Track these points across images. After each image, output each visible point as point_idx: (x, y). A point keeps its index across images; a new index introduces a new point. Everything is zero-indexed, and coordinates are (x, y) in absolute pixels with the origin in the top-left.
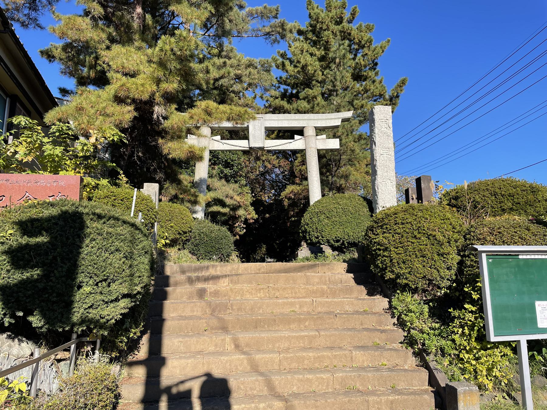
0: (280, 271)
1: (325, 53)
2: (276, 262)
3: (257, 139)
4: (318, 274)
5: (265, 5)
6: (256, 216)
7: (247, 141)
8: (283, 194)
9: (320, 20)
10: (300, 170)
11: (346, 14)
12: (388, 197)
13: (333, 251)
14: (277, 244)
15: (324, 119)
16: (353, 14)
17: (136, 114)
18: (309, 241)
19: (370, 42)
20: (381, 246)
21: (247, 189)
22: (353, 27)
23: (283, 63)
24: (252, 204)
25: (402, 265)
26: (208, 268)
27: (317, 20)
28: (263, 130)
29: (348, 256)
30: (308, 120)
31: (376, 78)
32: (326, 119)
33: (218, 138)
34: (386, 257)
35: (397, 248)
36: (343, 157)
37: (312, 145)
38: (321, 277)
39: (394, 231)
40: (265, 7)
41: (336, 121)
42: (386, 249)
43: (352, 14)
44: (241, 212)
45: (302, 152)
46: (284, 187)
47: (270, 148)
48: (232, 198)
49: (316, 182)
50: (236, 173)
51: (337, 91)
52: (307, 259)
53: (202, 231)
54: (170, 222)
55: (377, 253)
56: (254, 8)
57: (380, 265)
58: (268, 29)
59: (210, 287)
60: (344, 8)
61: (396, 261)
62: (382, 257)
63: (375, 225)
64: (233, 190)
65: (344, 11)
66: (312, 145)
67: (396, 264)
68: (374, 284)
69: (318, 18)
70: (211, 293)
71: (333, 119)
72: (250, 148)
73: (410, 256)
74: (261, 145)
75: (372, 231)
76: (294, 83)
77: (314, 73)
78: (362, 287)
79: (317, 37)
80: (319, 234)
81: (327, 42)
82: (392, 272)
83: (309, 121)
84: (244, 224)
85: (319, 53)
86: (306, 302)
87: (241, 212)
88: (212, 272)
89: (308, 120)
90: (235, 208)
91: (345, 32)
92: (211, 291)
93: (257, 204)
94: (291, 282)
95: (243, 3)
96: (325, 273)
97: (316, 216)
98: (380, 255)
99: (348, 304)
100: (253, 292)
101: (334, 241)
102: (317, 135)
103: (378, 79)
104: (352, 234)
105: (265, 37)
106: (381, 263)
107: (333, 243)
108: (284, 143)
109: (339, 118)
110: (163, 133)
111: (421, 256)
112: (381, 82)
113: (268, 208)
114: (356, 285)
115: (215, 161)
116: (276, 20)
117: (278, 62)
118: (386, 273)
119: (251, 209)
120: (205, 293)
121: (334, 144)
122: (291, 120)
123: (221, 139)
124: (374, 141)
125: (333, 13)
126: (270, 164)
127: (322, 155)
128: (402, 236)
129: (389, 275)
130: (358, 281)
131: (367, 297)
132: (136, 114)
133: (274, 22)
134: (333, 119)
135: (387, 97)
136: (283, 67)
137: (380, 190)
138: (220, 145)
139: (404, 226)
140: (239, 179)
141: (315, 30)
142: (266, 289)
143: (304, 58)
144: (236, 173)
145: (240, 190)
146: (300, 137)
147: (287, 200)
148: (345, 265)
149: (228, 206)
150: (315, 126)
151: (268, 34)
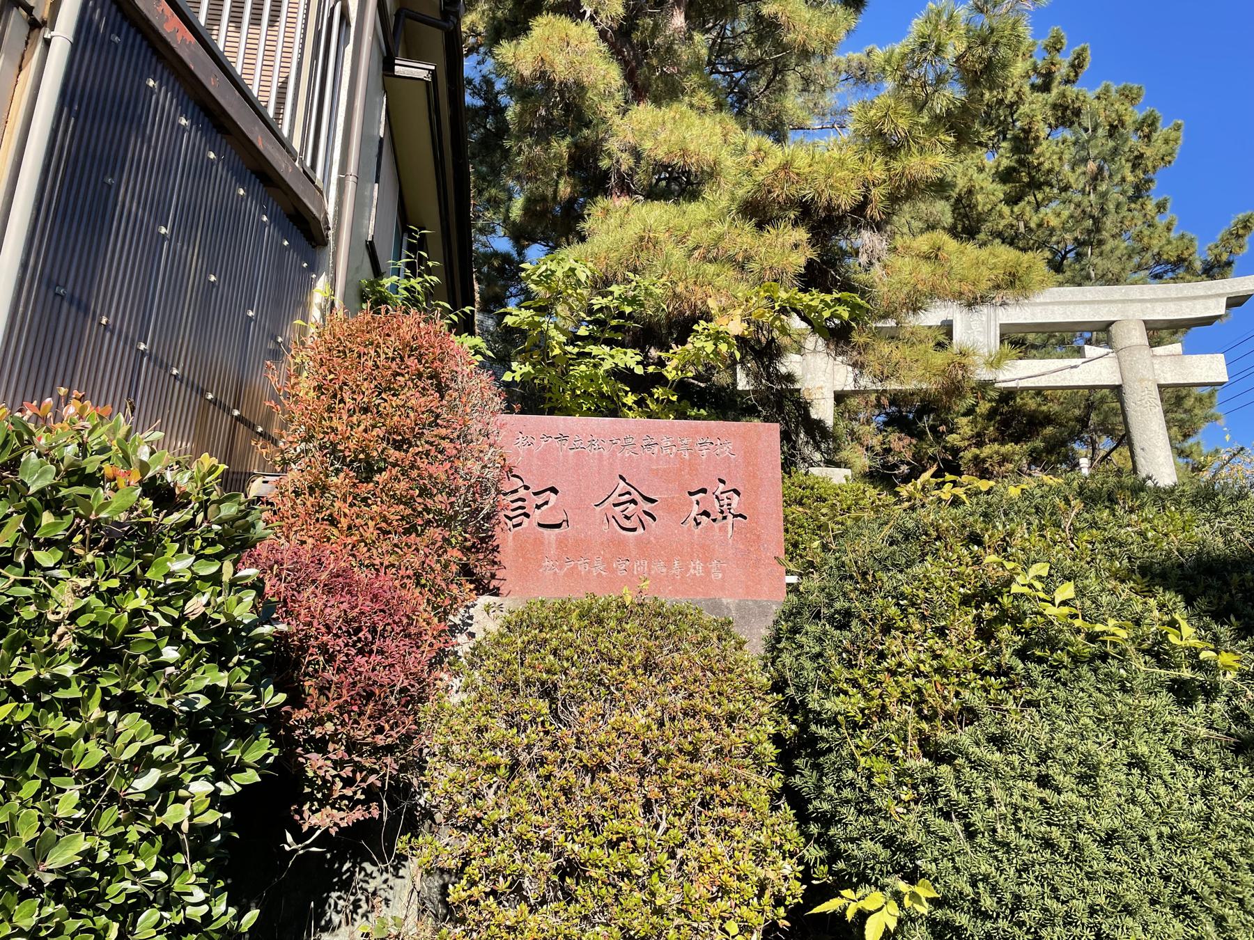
15: (1173, 300)
30: (1123, 301)
47: (1012, 384)
60: (1058, 50)
65: (1058, 58)
71: (1202, 299)
81: (1027, 131)
83: (1136, 303)
89: (1123, 301)
91: (1067, 108)
109: (1219, 295)
121: (1209, 368)
122: (1070, 303)
127: (1175, 398)
135: (1198, 265)
150: (1146, 318)
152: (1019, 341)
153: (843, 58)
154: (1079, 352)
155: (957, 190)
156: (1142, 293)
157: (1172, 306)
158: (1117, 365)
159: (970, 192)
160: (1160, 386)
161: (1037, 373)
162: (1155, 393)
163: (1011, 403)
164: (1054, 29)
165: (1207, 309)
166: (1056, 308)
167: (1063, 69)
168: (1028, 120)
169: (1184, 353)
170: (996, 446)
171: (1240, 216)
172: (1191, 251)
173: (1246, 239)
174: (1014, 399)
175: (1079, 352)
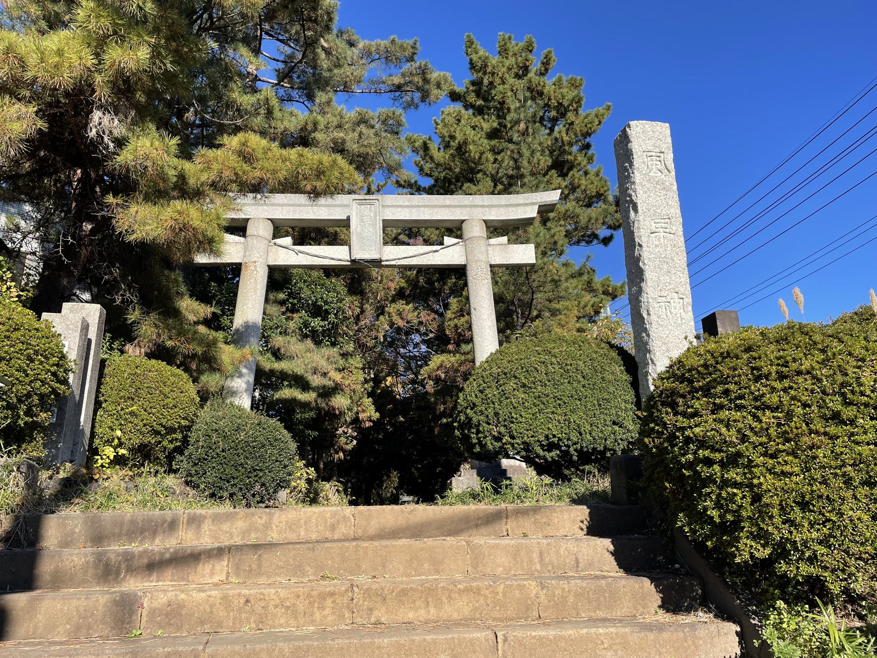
0: (394, 534)
1: (500, 124)
2: (417, 503)
3: (366, 244)
4: (505, 541)
5: (392, 37)
6: (376, 416)
7: (346, 248)
8: (424, 372)
9: (489, 70)
10: (456, 326)
11: (535, 61)
12: (671, 335)
13: (539, 474)
15: (503, 206)
16: (546, 64)
17: (42, 124)
18: (478, 449)
19: (579, 101)
20: (713, 449)
21: (357, 362)
22: (547, 82)
25: (797, 514)
26: (172, 525)
27: (484, 68)
28: (380, 225)
29: (580, 486)
30: (471, 206)
31: (589, 167)
32: (507, 206)
33: (288, 241)
34: (735, 485)
35: (773, 456)
36: (538, 296)
37: (483, 258)
38: (517, 550)
39: (756, 399)
40: (393, 41)
41: (528, 208)
42: (733, 460)
43: (543, 63)
45: (460, 272)
48: (325, 375)
49: (488, 331)
50: (335, 326)
51: (522, 176)
52: (474, 496)
53: (215, 426)
54: (129, 402)
55: (697, 474)
56: (373, 43)
57: (714, 513)
58: (397, 80)
59: (156, 592)
60: (531, 51)
61: (776, 500)
62: (721, 488)
63: (683, 388)
64: (328, 359)
65: (530, 57)
66: (483, 258)
67: (775, 512)
68: (676, 573)
69: (486, 66)
70: (153, 612)
71: (522, 206)
72: (353, 261)
73: (825, 482)
74: (374, 255)
75: (673, 405)
76: (445, 178)
77: (480, 158)
78: (646, 582)
79: (485, 100)
80: (503, 430)
81: (502, 103)
82: (761, 536)
83: (474, 208)
85: (489, 123)
86: (472, 642)
88: (186, 539)
89: (471, 206)
90: (326, 393)
92: (155, 604)
93: (382, 398)
94: (426, 565)
95: (355, 37)
96: (525, 535)
97: (494, 384)
98: (711, 480)
99: (610, 648)
100: (301, 607)
101: (542, 446)
102: (489, 238)
103: (592, 169)
104: (588, 427)
105: (392, 95)
106: (718, 505)
107: (541, 453)
108: (421, 252)
109: (533, 204)
110: (125, 185)
111: (864, 483)
112: (597, 175)
113: (403, 405)
114: (621, 573)
115: (293, 305)
116: (412, 63)
117: (417, 144)
118: (738, 540)
119: (368, 401)
120: (132, 612)
121: (524, 254)
122: (435, 206)
123: (294, 244)
124: (632, 201)
125: (511, 61)
126: (402, 319)
128: (789, 415)
129: (748, 549)
130: (629, 562)
131: (664, 617)
132: (42, 124)
133: (407, 67)
135: (611, 198)
136: (425, 151)
137: (653, 317)
138: (290, 255)
139: (786, 383)
141: (480, 89)
142: (342, 595)
143: (462, 131)
144: (335, 326)
145: (341, 362)
146: (456, 240)
148: (583, 512)
149: (314, 389)
150: (485, 218)
151: (399, 88)
153: (373, 43)
155: (457, 142)
156: (483, 201)
158: (464, 250)
159: (465, 143)
160: (491, 266)
161: (411, 255)
164: (527, 37)
165: (525, 212)
167: (535, 66)
168: (502, 95)
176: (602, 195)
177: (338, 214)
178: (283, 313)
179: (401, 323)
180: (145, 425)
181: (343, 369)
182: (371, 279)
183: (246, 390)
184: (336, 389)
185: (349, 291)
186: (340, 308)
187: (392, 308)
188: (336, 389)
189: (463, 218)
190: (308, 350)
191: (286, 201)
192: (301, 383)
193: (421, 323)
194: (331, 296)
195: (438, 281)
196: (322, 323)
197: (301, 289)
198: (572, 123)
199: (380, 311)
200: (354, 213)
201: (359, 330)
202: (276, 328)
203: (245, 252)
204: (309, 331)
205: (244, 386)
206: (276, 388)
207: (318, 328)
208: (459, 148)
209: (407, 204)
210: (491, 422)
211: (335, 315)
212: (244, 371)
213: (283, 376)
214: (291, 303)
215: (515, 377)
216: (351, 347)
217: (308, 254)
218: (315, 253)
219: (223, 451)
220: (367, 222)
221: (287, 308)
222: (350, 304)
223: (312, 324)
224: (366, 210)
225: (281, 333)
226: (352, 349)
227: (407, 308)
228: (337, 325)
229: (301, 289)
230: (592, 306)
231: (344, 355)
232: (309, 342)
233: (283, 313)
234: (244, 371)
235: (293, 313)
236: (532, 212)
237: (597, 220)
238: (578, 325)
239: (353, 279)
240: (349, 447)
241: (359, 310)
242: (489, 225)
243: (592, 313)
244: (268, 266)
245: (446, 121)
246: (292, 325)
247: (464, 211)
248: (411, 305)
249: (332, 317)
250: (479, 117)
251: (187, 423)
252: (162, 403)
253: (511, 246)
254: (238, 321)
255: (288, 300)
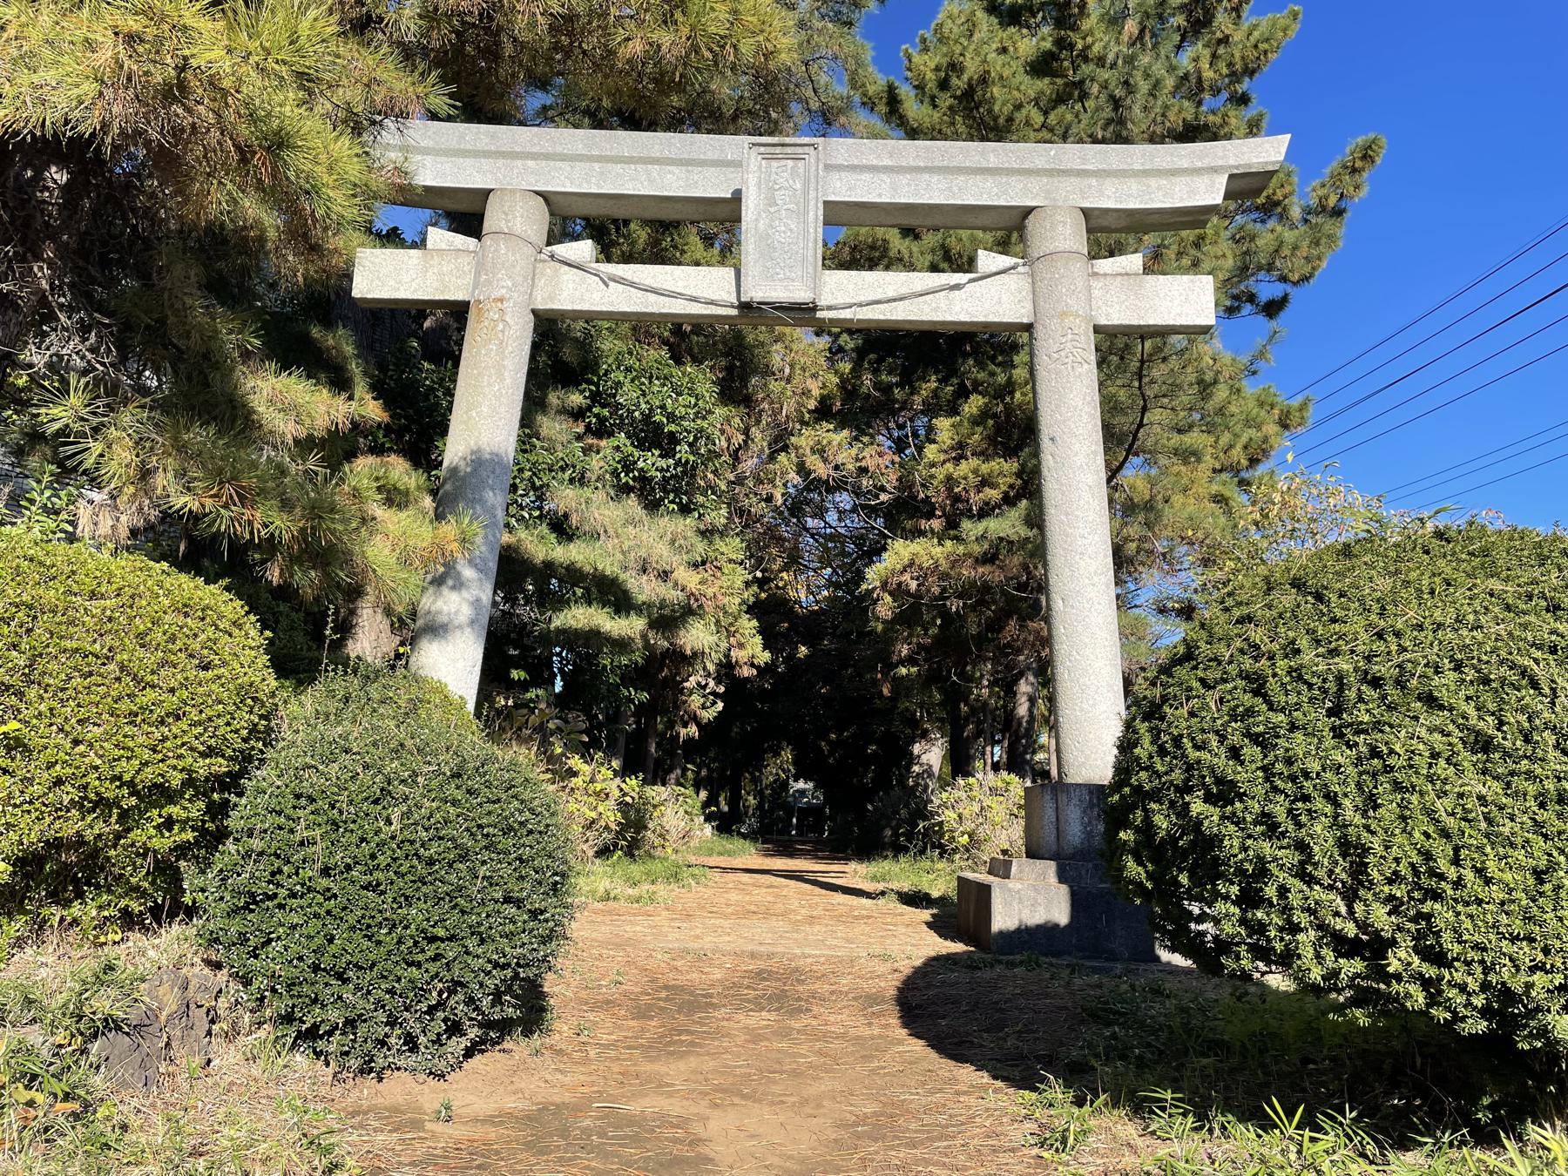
3: (780, 261)
6: (764, 657)
7: (728, 273)
8: (873, 575)
10: (949, 478)
14: (830, 742)
21: (732, 547)
23: (891, 89)
24: (754, 609)
28: (816, 214)
30: (1051, 173)
32: (1146, 173)
36: (1154, 415)
37: (1065, 306)
41: (1202, 182)
44: (697, 636)
45: (996, 348)
46: (875, 551)
48: (664, 575)
49: (1086, 496)
50: (689, 471)
64: (673, 542)
71: (1191, 178)
72: (746, 307)
83: (1063, 178)
84: (718, 681)
87: (697, 636)
89: (1051, 173)
90: (668, 619)
93: (771, 612)
102: (1093, 256)
108: (919, 288)
109: (1214, 170)
113: (810, 626)
115: (601, 420)
119: (749, 625)
121: (1187, 299)
126: (825, 460)
127: (1120, 350)
134: (1191, 178)
135: (1296, 213)
138: (587, 285)
140: (701, 499)
143: (977, 53)
144: (689, 471)
145: (700, 547)
146: (1004, 261)
147: (888, 599)
152: (859, 241)
154: (968, 265)
155: (965, 77)
157: (1134, 185)
158: (1028, 287)
159: (984, 80)
160: (1097, 329)
161: (891, 294)
162: (1088, 341)
163: (1008, 399)
165: (1192, 192)
166: (935, 178)
169: (1147, 270)
170: (974, 462)
171: (1360, 140)
172: (1288, 189)
173: (1365, 175)
174: (1012, 393)
175: (968, 265)
176: (1278, 203)
177: (714, 187)
178: (579, 438)
179: (821, 470)
180: (59, 782)
181: (704, 563)
182: (767, 372)
183: (472, 623)
184: (687, 612)
185: (722, 394)
186: (701, 430)
187: (804, 440)
188: (687, 612)
189: (1034, 204)
190: (631, 521)
191: (581, 149)
192: (611, 593)
193: (863, 471)
194: (681, 405)
195: (900, 385)
196: (662, 463)
197: (618, 384)
198: (1225, 40)
199: (780, 442)
200: (752, 181)
201: (740, 481)
202: (563, 469)
203: (478, 274)
204: (634, 479)
205: (466, 612)
206: (560, 603)
207: (653, 473)
208: (969, 93)
209: (887, 162)
210: (1321, 873)
211: (690, 445)
212: (468, 573)
213: (573, 575)
214: (596, 416)
215: (1431, 701)
216: (719, 517)
217: (632, 284)
218: (650, 282)
219: (326, 872)
220: (784, 222)
221: (588, 428)
222: (723, 423)
223: (641, 464)
224: (785, 173)
225: (572, 481)
226: (723, 521)
227: (836, 437)
228: (694, 468)
229: (618, 384)
230: (1246, 447)
231: (706, 534)
232: (632, 504)
233: (579, 438)
234: (468, 573)
235: (601, 438)
236: (1211, 193)
237: (1295, 248)
238: (1215, 488)
239: (729, 369)
240: (708, 715)
241: (741, 438)
242: (1093, 223)
243: (1245, 462)
244: (534, 311)
245: (946, 30)
246: (596, 464)
247: (1035, 184)
248: (845, 433)
249: (683, 451)
250: (1012, 29)
251: (220, 766)
252: (125, 706)
253: (1151, 279)
254: (455, 450)
255: (589, 408)
